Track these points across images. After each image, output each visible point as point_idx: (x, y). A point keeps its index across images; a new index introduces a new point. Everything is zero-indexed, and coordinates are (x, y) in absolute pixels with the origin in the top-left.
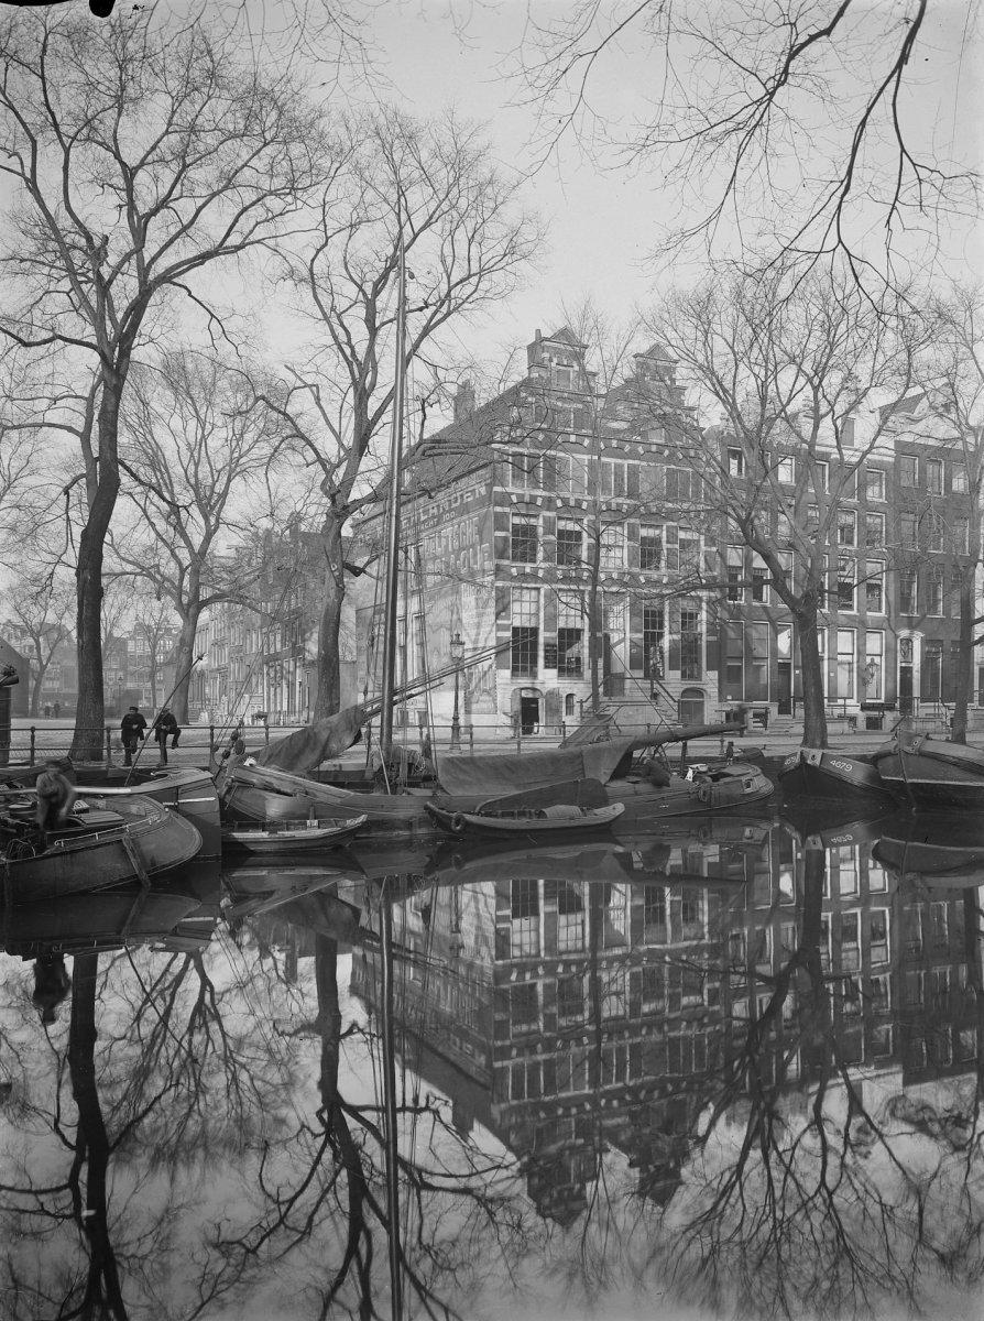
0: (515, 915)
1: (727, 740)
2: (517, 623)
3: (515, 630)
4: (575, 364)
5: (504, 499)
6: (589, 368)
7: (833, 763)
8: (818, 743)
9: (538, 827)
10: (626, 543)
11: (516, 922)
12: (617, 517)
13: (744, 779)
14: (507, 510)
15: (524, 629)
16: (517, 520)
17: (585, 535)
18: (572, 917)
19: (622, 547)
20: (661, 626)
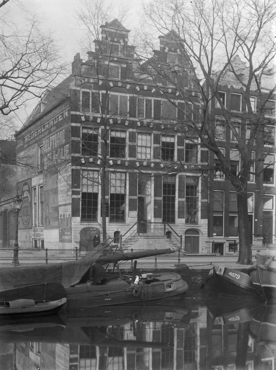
0: (82, 356)
1: (134, 261)
2: (85, 190)
3: (84, 195)
4: (121, 41)
5: (76, 119)
6: (129, 44)
7: (230, 274)
8: (246, 261)
9: (22, 311)
10: (153, 145)
11: (82, 362)
12: (146, 129)
13: (166, 283)
14: (78, 125)
15: (90, 194)
16: (85, 131)
17: (100, 138)
18: (116, 359)
19: (150, 148)
20: (174, 193)
